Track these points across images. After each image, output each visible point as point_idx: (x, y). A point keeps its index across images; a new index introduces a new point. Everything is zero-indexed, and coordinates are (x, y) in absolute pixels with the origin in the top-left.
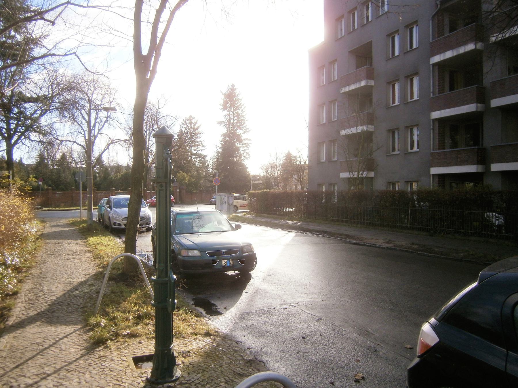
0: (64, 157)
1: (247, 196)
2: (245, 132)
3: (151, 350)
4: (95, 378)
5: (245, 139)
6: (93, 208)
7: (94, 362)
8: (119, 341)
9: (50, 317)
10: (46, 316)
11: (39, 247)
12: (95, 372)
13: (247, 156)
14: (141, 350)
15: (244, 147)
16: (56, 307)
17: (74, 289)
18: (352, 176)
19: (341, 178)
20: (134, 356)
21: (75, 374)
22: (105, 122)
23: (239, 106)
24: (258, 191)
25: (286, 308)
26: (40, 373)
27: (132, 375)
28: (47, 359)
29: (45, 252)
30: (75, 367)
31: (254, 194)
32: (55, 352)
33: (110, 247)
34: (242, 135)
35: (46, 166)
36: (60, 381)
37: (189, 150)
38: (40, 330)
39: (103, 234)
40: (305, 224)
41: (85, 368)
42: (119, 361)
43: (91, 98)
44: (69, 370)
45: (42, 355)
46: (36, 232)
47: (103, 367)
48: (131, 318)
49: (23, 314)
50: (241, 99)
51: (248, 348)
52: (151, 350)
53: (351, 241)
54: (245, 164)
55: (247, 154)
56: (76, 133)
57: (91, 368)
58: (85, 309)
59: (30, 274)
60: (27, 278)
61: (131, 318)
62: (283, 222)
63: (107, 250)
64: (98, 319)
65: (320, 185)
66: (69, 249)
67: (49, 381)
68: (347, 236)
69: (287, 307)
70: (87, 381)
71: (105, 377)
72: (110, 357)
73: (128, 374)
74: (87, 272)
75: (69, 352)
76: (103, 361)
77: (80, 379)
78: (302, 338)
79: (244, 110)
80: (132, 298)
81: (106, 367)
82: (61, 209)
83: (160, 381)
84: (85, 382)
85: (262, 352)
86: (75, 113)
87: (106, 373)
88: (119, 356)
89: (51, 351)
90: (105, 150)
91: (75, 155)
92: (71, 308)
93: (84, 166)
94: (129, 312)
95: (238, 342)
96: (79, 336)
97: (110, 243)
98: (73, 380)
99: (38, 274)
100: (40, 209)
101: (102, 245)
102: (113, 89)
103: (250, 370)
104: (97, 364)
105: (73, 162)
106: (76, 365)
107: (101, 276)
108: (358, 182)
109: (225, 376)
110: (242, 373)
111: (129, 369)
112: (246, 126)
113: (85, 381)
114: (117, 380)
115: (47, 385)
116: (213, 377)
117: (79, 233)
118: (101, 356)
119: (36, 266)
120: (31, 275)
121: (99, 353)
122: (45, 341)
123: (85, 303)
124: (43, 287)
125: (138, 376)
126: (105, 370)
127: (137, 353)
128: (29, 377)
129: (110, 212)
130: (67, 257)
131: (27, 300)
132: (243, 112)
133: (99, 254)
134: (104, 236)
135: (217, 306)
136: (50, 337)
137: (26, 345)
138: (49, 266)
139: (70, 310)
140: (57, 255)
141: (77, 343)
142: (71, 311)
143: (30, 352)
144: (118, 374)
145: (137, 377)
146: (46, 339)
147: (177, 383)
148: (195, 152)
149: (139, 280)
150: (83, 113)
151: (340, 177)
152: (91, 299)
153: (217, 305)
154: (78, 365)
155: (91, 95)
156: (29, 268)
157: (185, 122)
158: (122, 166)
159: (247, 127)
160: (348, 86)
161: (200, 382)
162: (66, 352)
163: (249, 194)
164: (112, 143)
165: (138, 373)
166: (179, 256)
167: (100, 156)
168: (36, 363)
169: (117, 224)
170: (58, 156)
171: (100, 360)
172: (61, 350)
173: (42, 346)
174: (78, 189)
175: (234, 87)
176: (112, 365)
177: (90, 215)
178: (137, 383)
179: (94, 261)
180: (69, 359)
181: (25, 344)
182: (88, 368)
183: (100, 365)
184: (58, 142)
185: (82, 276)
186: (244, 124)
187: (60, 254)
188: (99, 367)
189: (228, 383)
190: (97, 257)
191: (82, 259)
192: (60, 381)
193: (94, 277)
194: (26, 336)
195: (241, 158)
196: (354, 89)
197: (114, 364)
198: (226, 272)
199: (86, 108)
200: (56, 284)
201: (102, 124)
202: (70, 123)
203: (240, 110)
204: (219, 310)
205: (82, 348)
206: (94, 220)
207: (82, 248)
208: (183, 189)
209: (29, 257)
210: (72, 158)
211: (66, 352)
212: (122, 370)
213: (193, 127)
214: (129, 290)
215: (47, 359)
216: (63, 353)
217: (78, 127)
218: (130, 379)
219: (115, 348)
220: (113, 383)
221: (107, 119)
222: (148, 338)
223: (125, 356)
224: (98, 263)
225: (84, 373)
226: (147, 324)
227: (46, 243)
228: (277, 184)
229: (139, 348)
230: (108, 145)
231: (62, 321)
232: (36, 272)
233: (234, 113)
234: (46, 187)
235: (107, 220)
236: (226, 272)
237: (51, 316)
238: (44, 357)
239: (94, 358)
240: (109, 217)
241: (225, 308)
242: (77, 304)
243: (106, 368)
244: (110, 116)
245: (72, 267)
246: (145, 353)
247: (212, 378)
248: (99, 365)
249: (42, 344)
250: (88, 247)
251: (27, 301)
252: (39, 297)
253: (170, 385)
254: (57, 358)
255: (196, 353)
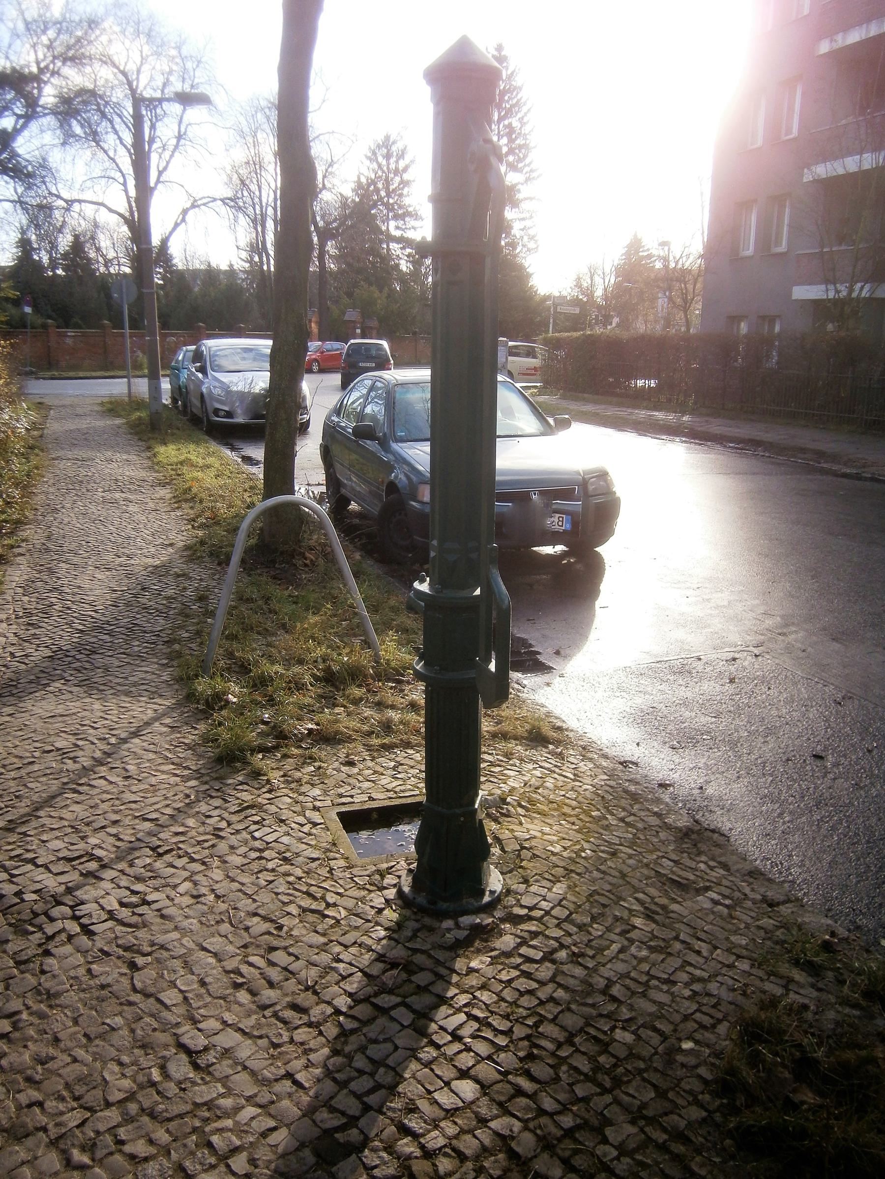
0: (77, 246)
1: (538, 347)
2: (527, 180)
3: (388, 791)
4: (243, 884)
5: (526, 199)
6: (161, 373)
7: (229, 824)
8: (289, 757)
9: (86, 669)
10: (73, 666)
11: (37, 468)
12: (235, 860)
13: (531, 245)
14: (360, 788)
15: (523, 219)
16: (96, 637)
17: (139, 587)
18: (831, 295)
19: (796, 300)
20: (343, 809)
21: (179, 863)
22: (173, 152)
23: (512, 106)
24: (569, 334)
25: (734, 659)
26: (76, 854)
27: (351, 878)
28: (91, 807)
29: (52, 481)
30: (175, 840)
31: (558, 340)
32: (111, 783)
33: (212, 473)
34: (519, 187)
35: (38, 266)
36: (138, 887)
37: (384, 228)
38: (61, 710)
39: (190, 439)
40: (698, 419)
41: (206, 845)
42: (302, 825)
43: (135, 84)
44: (160, 850)
45: (75, 791)
46: (27, 429)
47: (257, 844)
48: (307, 679)
49: (12, 654)
50: (520, 88)
51: (661, 785)
52: (388, 791)
53: (835, 467)
54: (526, 265)
55: (532, 238)
56: (104, 180)
57: (223, 847)
58: (177, 647)
59: (23, 541)
60: (16, 550)
61: (307, 679)
62: (642, 414)
63: (208, 479)
64: (219, 685)
65: (734, 319)
66: (111, 474)
67: (106, 885)
68: (820, 455)
69: (737, 656)
70: (218, 892)
71: (271, 882)
72: (273, 809)
73: (341, 875)
74: (164, 537)
75: (152, 786)
76: (255, 823)
77: (195, 884)
78: (815, 756)
79: (525, 120)
80: (309, 623)
81: (268, 843)
82: (81, 374)
83: (444, 906)
84: (212, 897)
85: (709, 798)
86: (98, 125)
87: (270, 865)
88: (298, 808)
89: (101, 778)
90: (177, 225)
91: (104, 242)
92: (137, 643)
93: (128, 270)
94: (301, 662)
95: (625, 762)
96: (172, 732)
97: (211, 460)
98: (175, 887)
99: (42, 541)
100: (32, 373)
101: (192, 465)
102: (191, 57)
103: (702, 866)
104: (238, 832)
105: (101, 259)
106: (177, 834)
107: (204, 551)
108: (847, 310)
109: (636, 890)
110: (679, 876)
111: (338, 856)
112: (530, 163)
113: (213, 890)
114: (308, 894)
115: (101, 901)
116: (603, 895)
117: (131, 434)
118: (246, 805)
119: (36, 521)
120: (23, 545)
121: (239, 795)
122: (80, 743)
123: (173, 629)
124: (59, 578)
125: (370, 884)
126: (266, 854)
127: (349, 799)
128: (46, 867)
129: (202, 383)
130: (108, 495)
131: (21, 614)
132: (523, 124)
133: (190, 489)
134: (193, 442)
135: (531, 646)
136: (91, 731)
137: (28, 754)
138: (66, 520)
139: (136, 649)
140: (84, 490)
141: (170, 756)
142: (139, 651)
143: (41, 779)
144: (307, 873)
145: (368, 886)
146: (81, 739)
147: (498, 914)
148: (397, 233)
149: (306, 565)
150: (117, 127)
151: (794, 297)
152: (187, 616)
153: (532, 642)
154: (182, 833)
155: (134, 77)
156: (18, 522)
157: (374, 153)
158: (219, 271)
159: (533, 166)
160: (841, 34)
161: (571, 914)
162: (142, 787)
163: (546, 342)
164: (193, 206)
165: (367, 873)
166: (414, 503)
167: (164, 242)
168: (61, 819)
169: (223, 413)
170: (65, 242)
171: (246, 817)
172: (127, 778)
173: (74, 759)
174: (120, 325)
175: (503, 53)
176: (285, 840)
177: (155, 390)
178: (372, 907)
179: (178, 508)
180: (155, 811)
181: (26, 750)
182: (213, 846)
183: (249, 837)
184: (61, 203)
185: (153, 550)
186: (525, 156)
187: (89, 487)
188: (246, 842)
189: (657, 917)
190: (184, 497)
191: (147, 503)
192: (138, 887)
193: (185, 553)
194: (25, 725)
195: (515, 248)
196: (858, 43)
197: (289, 834)
198: (534, 549)
199: (125, 113)
200: (90, 569)
201: (167, 155)
202: (88, 153)
203: (517, 118)
204: (541, 658)
205: (186, 772)
206: (164, 401)
207: (143, 474)
208: (371, 328)
209: (17, 493)
210: (98, 249)
211: (142, 787)
212: (318, 859)
213: (393, 166)
214: (286, 593)
215: (91, 807)
216: (134, 789)
217: (108, 164)
218: (347, 893)
219: (282, 779)
220: (300, 907)
221: (178, 141)
222: (369, 748)
223: (315, 809)
224: (187, 514)
225: (204, 863)
226: (356, 702)
227: (53, 459)
228: (607, 320)
229: (352, 781)
230: (185, 212)
231: (118, 680)
232: (36, 537)
233: (501, 126)
234: (40, 321)
235: (196, 402)
236: (534, 549)
237: (87, 665)
238: (82, 797)
239: (225, 810)
240: (202, 395)
241: (558, 653)
242: (152, 632)
243: (267, 849)
244: (185, 134)
245: (124, 524)
246: (374, 800)
247: (603, 900)
248: (245, 835)
249: (72, 755)
250: (158, 472)
251: (21, 617)
252: (52, 605)
253: (478, 921)
254: (117, 802)
255: (523, 804)
